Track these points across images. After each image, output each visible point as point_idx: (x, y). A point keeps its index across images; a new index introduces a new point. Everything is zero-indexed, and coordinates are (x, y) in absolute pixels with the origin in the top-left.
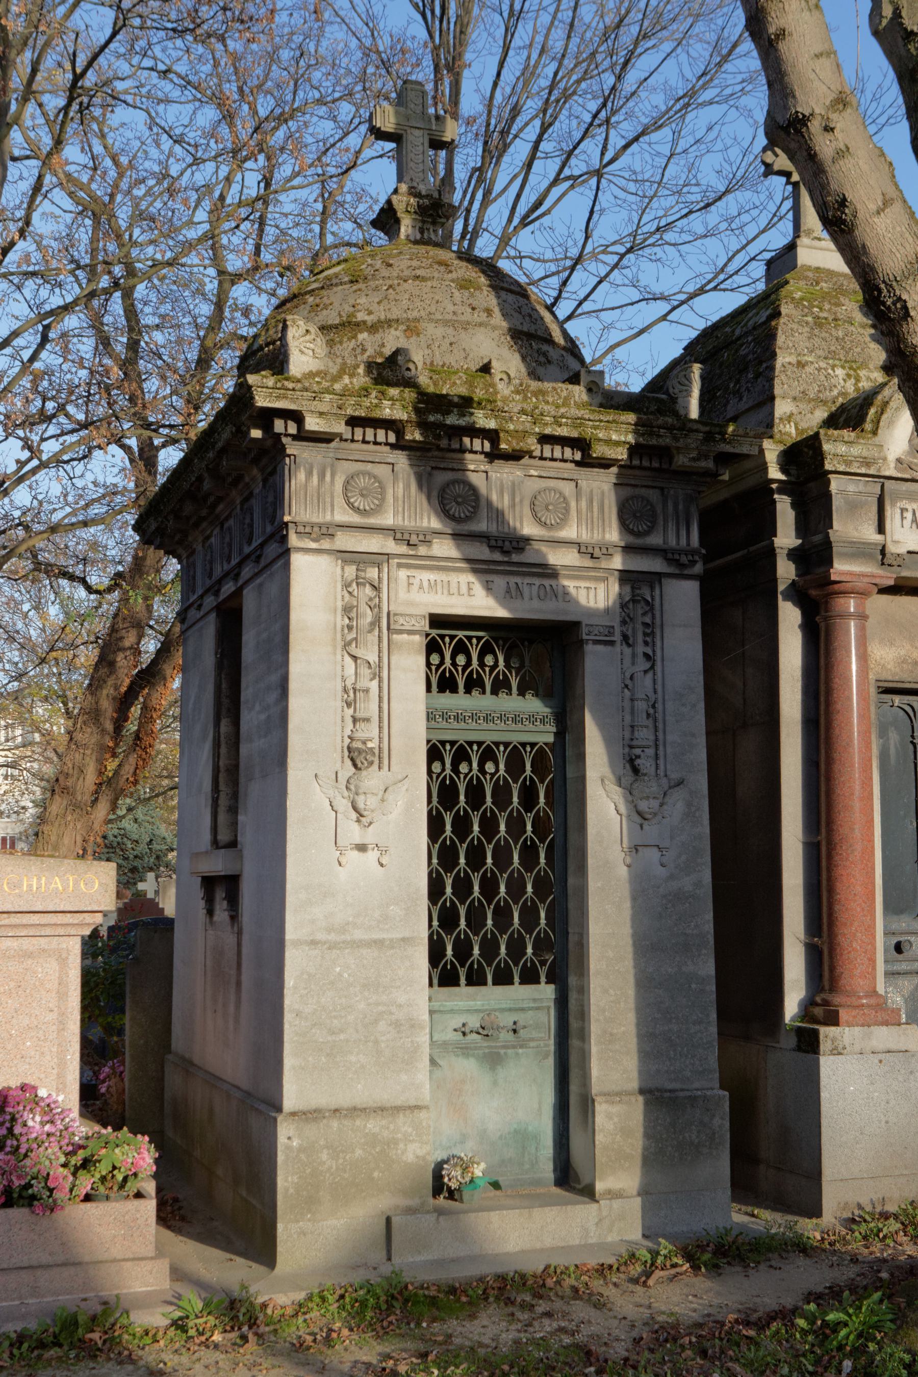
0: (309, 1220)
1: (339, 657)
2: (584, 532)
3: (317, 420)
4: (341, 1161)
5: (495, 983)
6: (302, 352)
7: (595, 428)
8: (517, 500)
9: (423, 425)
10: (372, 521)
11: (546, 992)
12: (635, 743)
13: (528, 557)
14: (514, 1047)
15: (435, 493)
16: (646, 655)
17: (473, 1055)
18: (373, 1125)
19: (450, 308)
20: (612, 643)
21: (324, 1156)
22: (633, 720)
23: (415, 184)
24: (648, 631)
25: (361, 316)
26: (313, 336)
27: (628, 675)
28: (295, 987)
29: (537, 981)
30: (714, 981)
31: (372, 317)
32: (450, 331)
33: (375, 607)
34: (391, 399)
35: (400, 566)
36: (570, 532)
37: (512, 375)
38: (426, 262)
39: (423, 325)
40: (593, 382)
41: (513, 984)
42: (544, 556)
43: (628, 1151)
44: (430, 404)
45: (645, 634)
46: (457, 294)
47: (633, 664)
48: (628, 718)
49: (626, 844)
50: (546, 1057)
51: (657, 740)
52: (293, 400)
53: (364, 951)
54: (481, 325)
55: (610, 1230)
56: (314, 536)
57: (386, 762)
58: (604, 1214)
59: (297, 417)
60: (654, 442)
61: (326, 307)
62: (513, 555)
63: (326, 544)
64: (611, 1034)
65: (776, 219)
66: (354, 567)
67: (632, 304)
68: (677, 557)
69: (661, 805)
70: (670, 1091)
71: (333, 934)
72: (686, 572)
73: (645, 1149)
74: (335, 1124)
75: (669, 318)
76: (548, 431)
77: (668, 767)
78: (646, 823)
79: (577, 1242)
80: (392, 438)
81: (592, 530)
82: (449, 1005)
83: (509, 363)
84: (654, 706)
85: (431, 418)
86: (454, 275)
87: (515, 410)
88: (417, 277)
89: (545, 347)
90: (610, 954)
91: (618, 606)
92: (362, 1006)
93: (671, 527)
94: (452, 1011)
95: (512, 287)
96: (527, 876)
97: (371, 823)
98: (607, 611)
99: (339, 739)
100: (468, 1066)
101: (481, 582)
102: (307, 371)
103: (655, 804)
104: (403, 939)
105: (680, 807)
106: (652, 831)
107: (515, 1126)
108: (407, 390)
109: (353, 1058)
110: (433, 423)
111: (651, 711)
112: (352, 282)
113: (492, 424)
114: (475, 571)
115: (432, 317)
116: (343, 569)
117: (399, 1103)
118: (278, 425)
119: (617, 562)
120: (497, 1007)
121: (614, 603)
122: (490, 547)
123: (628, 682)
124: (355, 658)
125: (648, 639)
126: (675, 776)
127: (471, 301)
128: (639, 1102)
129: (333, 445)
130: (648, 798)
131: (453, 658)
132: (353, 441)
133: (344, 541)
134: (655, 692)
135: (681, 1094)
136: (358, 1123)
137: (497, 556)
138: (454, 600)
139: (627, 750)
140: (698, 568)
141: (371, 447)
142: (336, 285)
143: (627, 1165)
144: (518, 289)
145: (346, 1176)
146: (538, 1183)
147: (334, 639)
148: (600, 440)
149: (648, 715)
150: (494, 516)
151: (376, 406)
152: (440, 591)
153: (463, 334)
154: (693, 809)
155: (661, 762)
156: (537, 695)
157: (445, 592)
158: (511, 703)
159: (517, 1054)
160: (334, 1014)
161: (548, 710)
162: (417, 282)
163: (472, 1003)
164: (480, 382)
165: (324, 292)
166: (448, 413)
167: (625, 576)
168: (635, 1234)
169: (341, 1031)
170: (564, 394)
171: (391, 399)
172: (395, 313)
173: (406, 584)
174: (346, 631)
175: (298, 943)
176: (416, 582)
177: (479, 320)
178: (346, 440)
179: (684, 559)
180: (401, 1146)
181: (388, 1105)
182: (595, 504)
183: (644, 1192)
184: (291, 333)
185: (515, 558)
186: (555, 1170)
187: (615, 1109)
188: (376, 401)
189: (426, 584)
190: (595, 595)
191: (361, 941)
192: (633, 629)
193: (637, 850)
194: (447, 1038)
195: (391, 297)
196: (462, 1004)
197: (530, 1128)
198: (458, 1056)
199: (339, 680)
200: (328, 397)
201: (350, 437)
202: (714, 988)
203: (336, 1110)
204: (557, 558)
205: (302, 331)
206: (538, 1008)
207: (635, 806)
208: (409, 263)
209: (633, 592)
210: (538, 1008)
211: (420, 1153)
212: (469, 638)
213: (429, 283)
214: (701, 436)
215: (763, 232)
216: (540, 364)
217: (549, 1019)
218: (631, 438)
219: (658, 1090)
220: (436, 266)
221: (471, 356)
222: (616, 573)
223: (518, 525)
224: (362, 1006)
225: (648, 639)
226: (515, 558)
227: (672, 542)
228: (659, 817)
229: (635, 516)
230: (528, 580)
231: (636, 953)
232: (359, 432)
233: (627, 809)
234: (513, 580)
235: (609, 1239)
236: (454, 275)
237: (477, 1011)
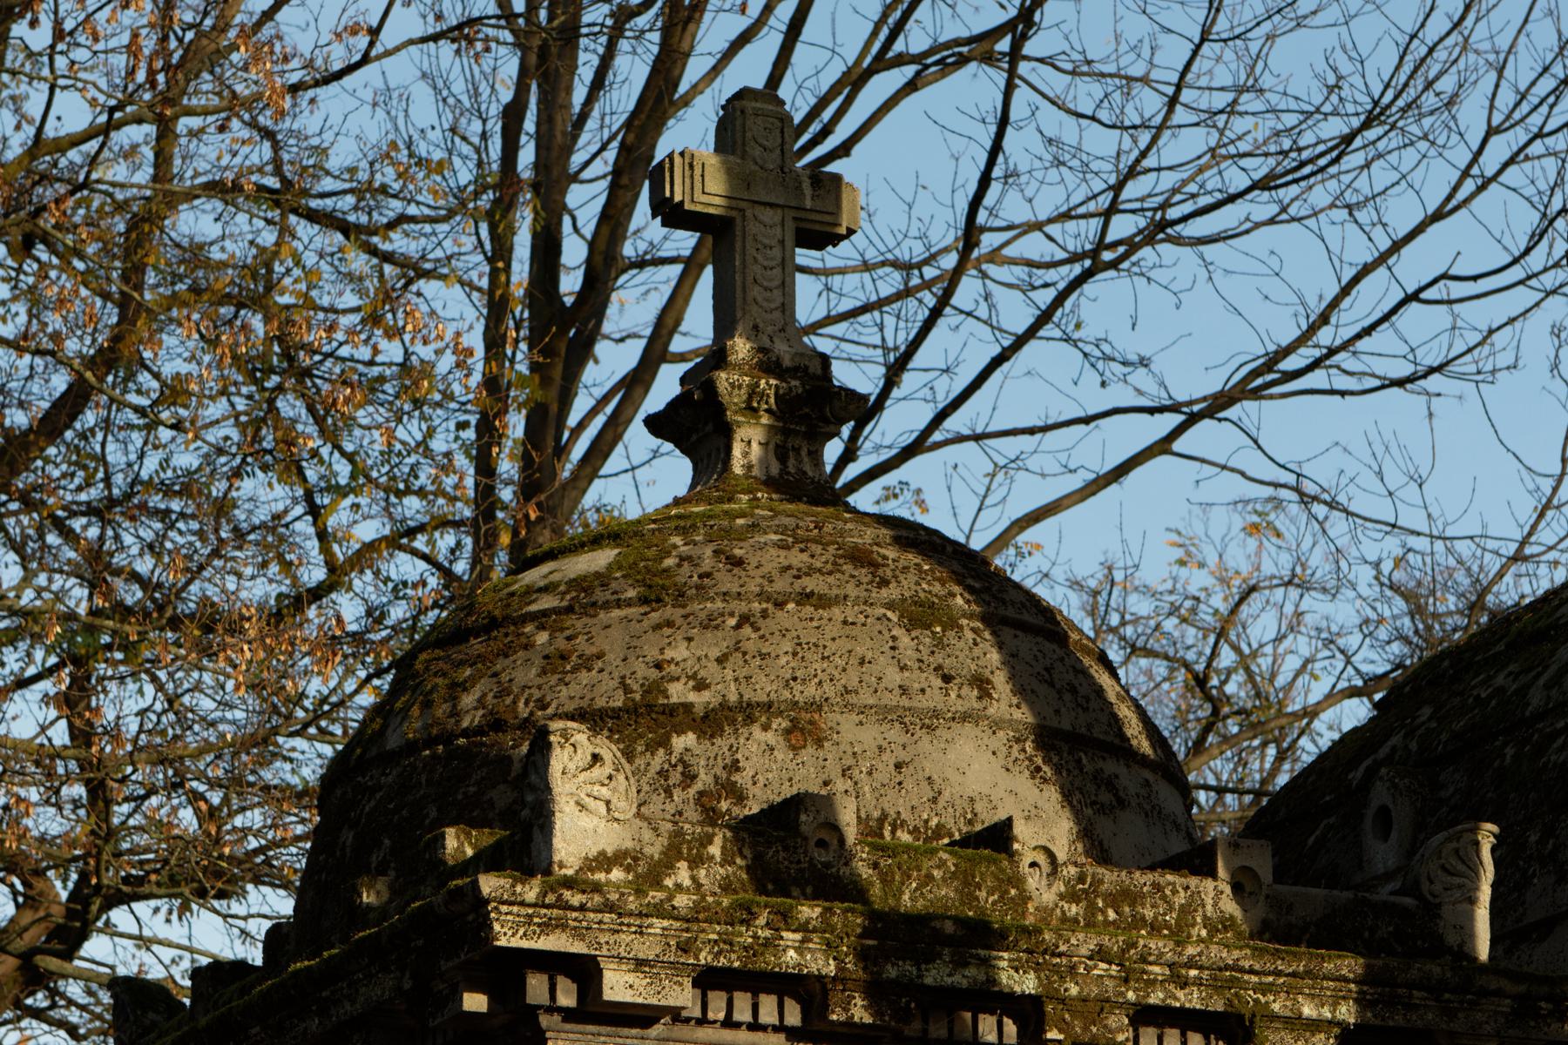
3: (630, 978)
6: (582, 807)
7: (1264, 989)
9: (876, 992)
19: (894, 677)
23: (766, 343)
25: (678, 692)
26: (608, 770)
31: (706, 696)
32: (895, 734)
34: (803, 928)
37: (1061, 856)
38: (824, 556)
39: (829, 718)
40: (1245, 869)
44: (894, 938)
46: (905, 641)
52: (578, 934)
54: (965, 717)
59: (585, 971)
60: (1399, 1020)
61: (586, 663)
65: (1469, 186)
67: (1087, 420)
75: (1177, 446)
76: (1156, 998)
80: (793, 1017)
83: (1045, 826)
85: (892, 972)
86: (892, 592)
87: (1084, 951)
88: (805, 598)
89: (1110, 767)
95: (1026, 617)
102: (593, 853)
108: (838, 907)
110: (895, 983)
112: (644, 601)
113: (1028, 984)
115: (852, 699)
118: (536, 987)
127: (939, 658)
129: (657, 1030)
132: (703, 1021)
141: (743, 1035)
142: (607, 606)
144: (1038, 621)
148: (1274, 1017)
151: (767, 943)
153: (925, 743)
162: (809, 609)
164: (985, 875)
165: (576, 623)
166: (930, 958)
170: (1180, 899)
171: (803, 928)
172: (763, 688)
177: (961, 706)
178: (687, 1020)
184: (561, 761)
188: (768, 933)
195: (750, 646)
200: (658, 924)
201: (697, 1013)
205: (583, 757)
208: (783, 558)
213: (837, 612)
214: (1506, 1005)
215: (1438, 216)
216: (1102, 809)
218: (1346, 1012)
220: (848, 568)
221: (946, 795)
232: (717, 1002)
236: (892, 592)
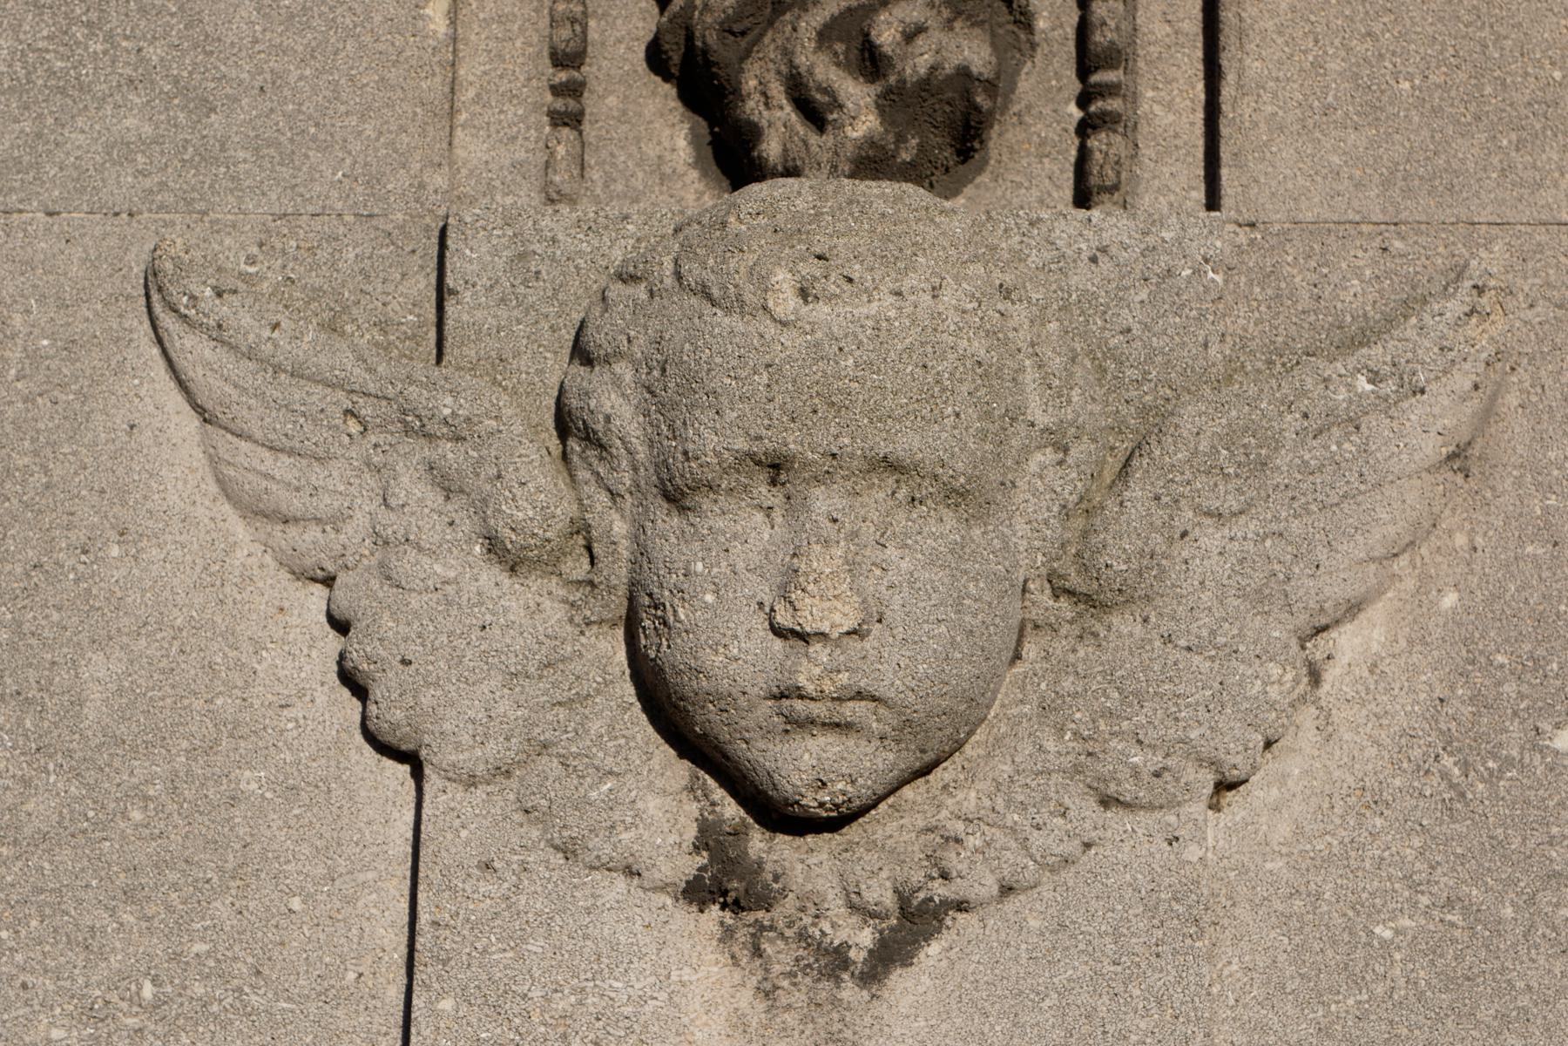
57: (1166, 101)
97: (914, 923)
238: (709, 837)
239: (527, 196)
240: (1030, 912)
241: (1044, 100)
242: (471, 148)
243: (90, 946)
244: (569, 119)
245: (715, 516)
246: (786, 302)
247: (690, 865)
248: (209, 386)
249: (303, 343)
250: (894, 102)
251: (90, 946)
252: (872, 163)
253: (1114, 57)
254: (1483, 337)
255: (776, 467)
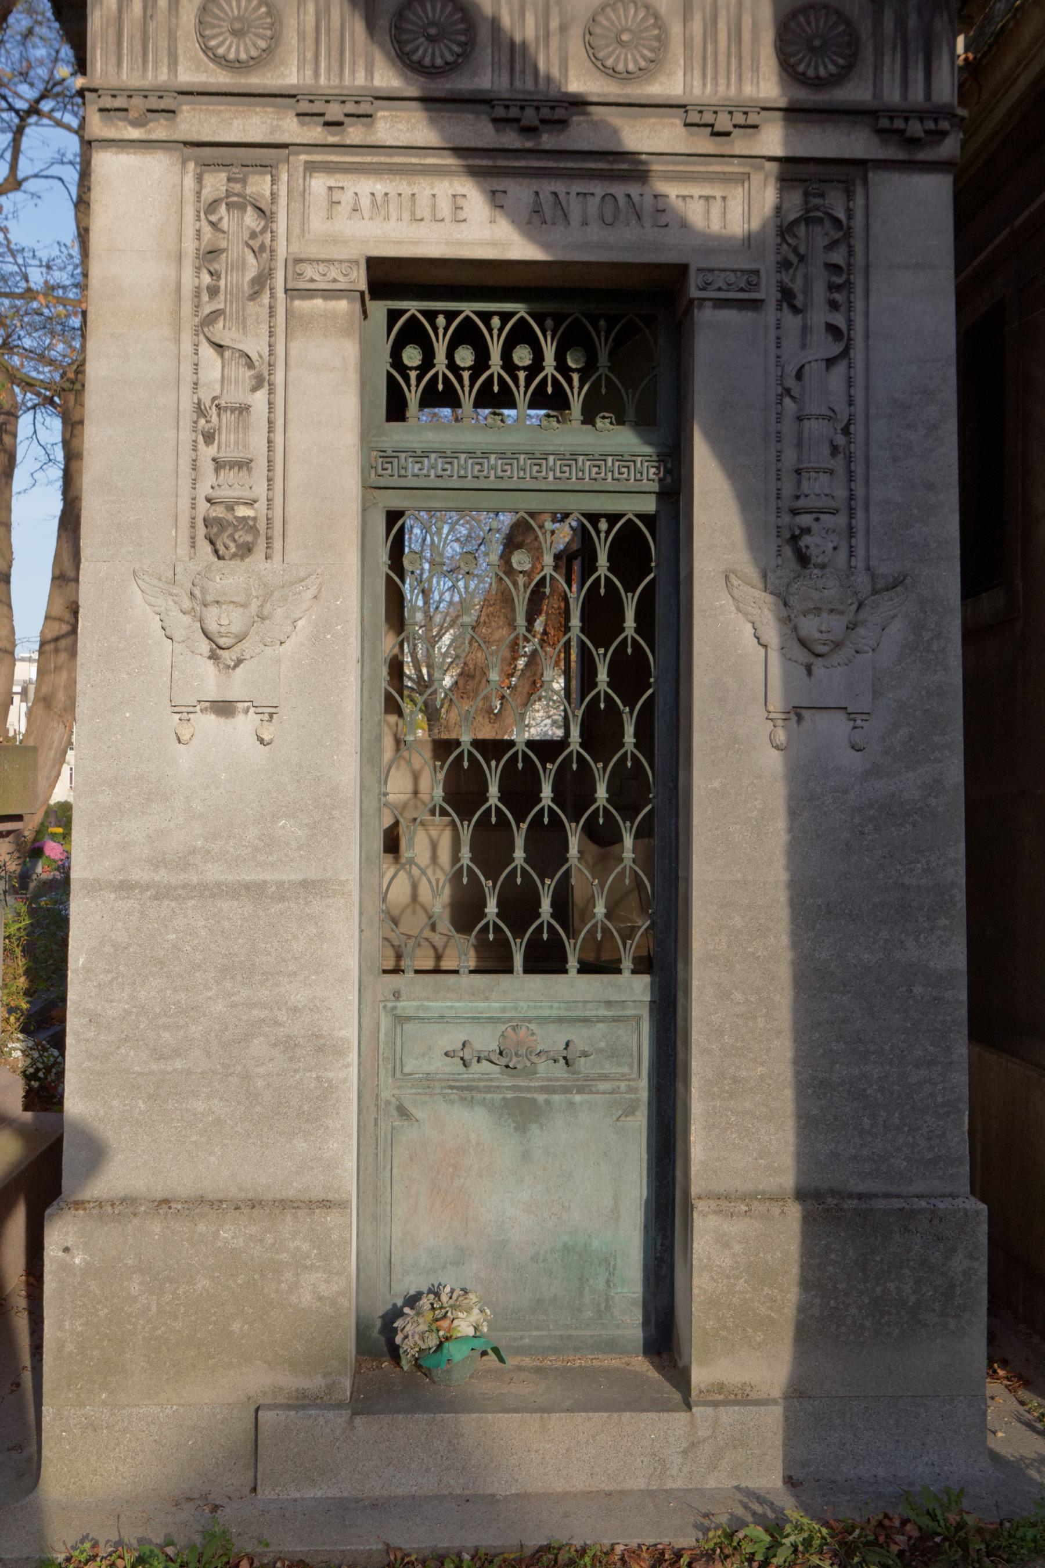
0: (104, 1403)
1: (187, 347)
2: (697, 83)
4: (167, 1297)
5: (530, 969)
8: (554, 24)
10: (255, 81)
11: (635, 989)
12: (801, 503)
13: (579, 136)
14: (566, 1090)
15: (383, 22)
16: (833, 330)
17: (483, 1103)
18: (230, 1233)
20: (755, 305)
21: (135, 1287)
22: (799, 460)
24: (839, 280)
27: (791, 370)
28: (87, 970)
29: (614, 968)
30: (964, 981)
33: (260, 247)
35: (311, 168)
36: (671, 85)
41: (565, 971)
42: (615, 132)
43: (763, 1310)
45: (832, 287)
47: (803, 346)
48: (790, 457)
49: (777, 703)
50: (631, 1110)
51: (851, 498)
53: (225, 905)
55: (714, 1467)
56: (133, 114)
57: (277, 545)
58: (702, 1433)
62: (545, 137)
63: (159, 130)
64: (736, 1080)
66: (223, 176)
68: (899, 124)
69: (852, 627)
70: (860, 1196)
71: (163, 871)
72: (921, 156)
73: (801, 1309)
74: (156, 1228)
77: (874, 551)
78: (818, 663)
79: (641, 1484)
81: (715, 78)
82: (436, 1006)
84: (846, 431)
90: (737, 921)
91: (772, 231)
92: (219, 1007)
93: (891, 64)
94: (442, 1019)
96: (597, 767)
97: (239, 662)
98: (749, 240)
99: (184, 503)
100: (472, 1124)
101: (484, 191)
103: (836, 624)
104: (304, 884)
105: (897, 629)
106: (831, 678)
107: (566, 1238)
109: (200, 1106)
111: (840, 440)
114: (474, 172)
116: (199, 179)
117: (290, 1193)
119: (772, 140)
120: (531, 1013)
121: (764, 226)
122: (495, 121)
123: (790, 382)
124: (219, 347)
125: (838, 297)
126: (886, 569)
128: (794, 1211)
130: (817, 611)
131: (450, 355)
133: (198, 122)
134: (851, 403)
135: (882, 1204)
136: (201, 1227)
137: (511, 139)
138: (422, 231)
139: (786, 519)
140: (950, 147)
143: (759, 1337)
145: (178, 1325)
146: (612, 1346)
147: (177, 312)
149: (835, 450)
150: (505, 59)
152: (394, 215)
154: (927, 635)
155: (859, 542)
156: (620, 422)
157: (406, 215)
158: (572, 435)
159: (572, 1104)
160: (163, 1020)
161: (648, 450)
163: (483, 1005)
167: (792, 170)
168: (769, 1479)
169: (177, 1053)
173: (325, 205)
174: (205, 297)
175: (94, 887)
176: (346, 199)
179: (915, 129)
180: (289, 1275)
181: (269, 1196)
182: (722, 26)
183: (798, 1393)
185: (548, 141)
186: (646, 1324)
187: (734, 1228)
189: (365, 202)
190: (726, 208)
191: (218, 885)
192: (806, 277)
193: (800, 718)
194: (433, 1068)
196: (461, 1006)
197: (596, 1244)
198: (452, 1102)
199: (186, 390)
202: (964, 996)
203: (166, 1201)
204: (640, 136)
206: (616, 1019)
207: (795, 629)
209: (806, 202)
210: (616, 1019)
211: (324, 1290)
212: (486, 317)
217: (640, 1039)
219: (834, 1193)
222: (772, 167)
223: (555, 72)
224: (219, 1007)
225: (838, 297)
226: (548, 141)
227: (893, 95)
228: (848, 651)
229: (812, 49)
230: (578, 186)
231: (795, 918)
233: (783, 635)
234: (547, 187)
235: (711, 1483)
237: (492, 1020)
238: (211, 650)
239: (187, 559)
240: (255, 660)
241: (262, 543)
242: (179, 551)
243: (129, 665)
244: (193, 547)
245: (210, 608)
246: (218, 580)
247: (209, 654)
248: (143, 588)
249: (155, 582)
250: (238, 547)
251: (129, 665)
252: (234, 556)
253: (271, 538)
254: (318, 581)
255: (218, 602)
